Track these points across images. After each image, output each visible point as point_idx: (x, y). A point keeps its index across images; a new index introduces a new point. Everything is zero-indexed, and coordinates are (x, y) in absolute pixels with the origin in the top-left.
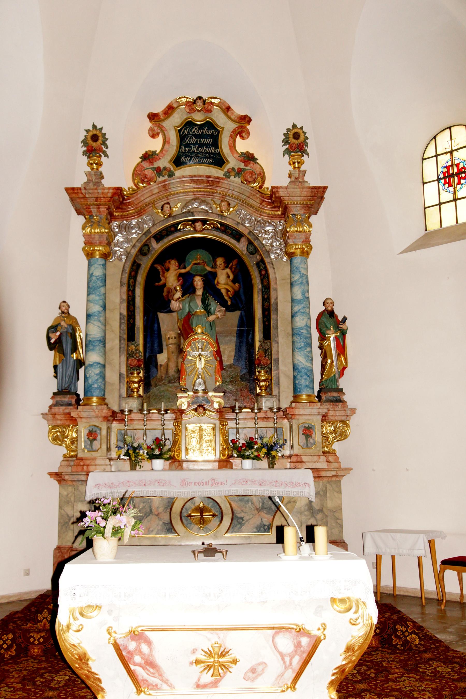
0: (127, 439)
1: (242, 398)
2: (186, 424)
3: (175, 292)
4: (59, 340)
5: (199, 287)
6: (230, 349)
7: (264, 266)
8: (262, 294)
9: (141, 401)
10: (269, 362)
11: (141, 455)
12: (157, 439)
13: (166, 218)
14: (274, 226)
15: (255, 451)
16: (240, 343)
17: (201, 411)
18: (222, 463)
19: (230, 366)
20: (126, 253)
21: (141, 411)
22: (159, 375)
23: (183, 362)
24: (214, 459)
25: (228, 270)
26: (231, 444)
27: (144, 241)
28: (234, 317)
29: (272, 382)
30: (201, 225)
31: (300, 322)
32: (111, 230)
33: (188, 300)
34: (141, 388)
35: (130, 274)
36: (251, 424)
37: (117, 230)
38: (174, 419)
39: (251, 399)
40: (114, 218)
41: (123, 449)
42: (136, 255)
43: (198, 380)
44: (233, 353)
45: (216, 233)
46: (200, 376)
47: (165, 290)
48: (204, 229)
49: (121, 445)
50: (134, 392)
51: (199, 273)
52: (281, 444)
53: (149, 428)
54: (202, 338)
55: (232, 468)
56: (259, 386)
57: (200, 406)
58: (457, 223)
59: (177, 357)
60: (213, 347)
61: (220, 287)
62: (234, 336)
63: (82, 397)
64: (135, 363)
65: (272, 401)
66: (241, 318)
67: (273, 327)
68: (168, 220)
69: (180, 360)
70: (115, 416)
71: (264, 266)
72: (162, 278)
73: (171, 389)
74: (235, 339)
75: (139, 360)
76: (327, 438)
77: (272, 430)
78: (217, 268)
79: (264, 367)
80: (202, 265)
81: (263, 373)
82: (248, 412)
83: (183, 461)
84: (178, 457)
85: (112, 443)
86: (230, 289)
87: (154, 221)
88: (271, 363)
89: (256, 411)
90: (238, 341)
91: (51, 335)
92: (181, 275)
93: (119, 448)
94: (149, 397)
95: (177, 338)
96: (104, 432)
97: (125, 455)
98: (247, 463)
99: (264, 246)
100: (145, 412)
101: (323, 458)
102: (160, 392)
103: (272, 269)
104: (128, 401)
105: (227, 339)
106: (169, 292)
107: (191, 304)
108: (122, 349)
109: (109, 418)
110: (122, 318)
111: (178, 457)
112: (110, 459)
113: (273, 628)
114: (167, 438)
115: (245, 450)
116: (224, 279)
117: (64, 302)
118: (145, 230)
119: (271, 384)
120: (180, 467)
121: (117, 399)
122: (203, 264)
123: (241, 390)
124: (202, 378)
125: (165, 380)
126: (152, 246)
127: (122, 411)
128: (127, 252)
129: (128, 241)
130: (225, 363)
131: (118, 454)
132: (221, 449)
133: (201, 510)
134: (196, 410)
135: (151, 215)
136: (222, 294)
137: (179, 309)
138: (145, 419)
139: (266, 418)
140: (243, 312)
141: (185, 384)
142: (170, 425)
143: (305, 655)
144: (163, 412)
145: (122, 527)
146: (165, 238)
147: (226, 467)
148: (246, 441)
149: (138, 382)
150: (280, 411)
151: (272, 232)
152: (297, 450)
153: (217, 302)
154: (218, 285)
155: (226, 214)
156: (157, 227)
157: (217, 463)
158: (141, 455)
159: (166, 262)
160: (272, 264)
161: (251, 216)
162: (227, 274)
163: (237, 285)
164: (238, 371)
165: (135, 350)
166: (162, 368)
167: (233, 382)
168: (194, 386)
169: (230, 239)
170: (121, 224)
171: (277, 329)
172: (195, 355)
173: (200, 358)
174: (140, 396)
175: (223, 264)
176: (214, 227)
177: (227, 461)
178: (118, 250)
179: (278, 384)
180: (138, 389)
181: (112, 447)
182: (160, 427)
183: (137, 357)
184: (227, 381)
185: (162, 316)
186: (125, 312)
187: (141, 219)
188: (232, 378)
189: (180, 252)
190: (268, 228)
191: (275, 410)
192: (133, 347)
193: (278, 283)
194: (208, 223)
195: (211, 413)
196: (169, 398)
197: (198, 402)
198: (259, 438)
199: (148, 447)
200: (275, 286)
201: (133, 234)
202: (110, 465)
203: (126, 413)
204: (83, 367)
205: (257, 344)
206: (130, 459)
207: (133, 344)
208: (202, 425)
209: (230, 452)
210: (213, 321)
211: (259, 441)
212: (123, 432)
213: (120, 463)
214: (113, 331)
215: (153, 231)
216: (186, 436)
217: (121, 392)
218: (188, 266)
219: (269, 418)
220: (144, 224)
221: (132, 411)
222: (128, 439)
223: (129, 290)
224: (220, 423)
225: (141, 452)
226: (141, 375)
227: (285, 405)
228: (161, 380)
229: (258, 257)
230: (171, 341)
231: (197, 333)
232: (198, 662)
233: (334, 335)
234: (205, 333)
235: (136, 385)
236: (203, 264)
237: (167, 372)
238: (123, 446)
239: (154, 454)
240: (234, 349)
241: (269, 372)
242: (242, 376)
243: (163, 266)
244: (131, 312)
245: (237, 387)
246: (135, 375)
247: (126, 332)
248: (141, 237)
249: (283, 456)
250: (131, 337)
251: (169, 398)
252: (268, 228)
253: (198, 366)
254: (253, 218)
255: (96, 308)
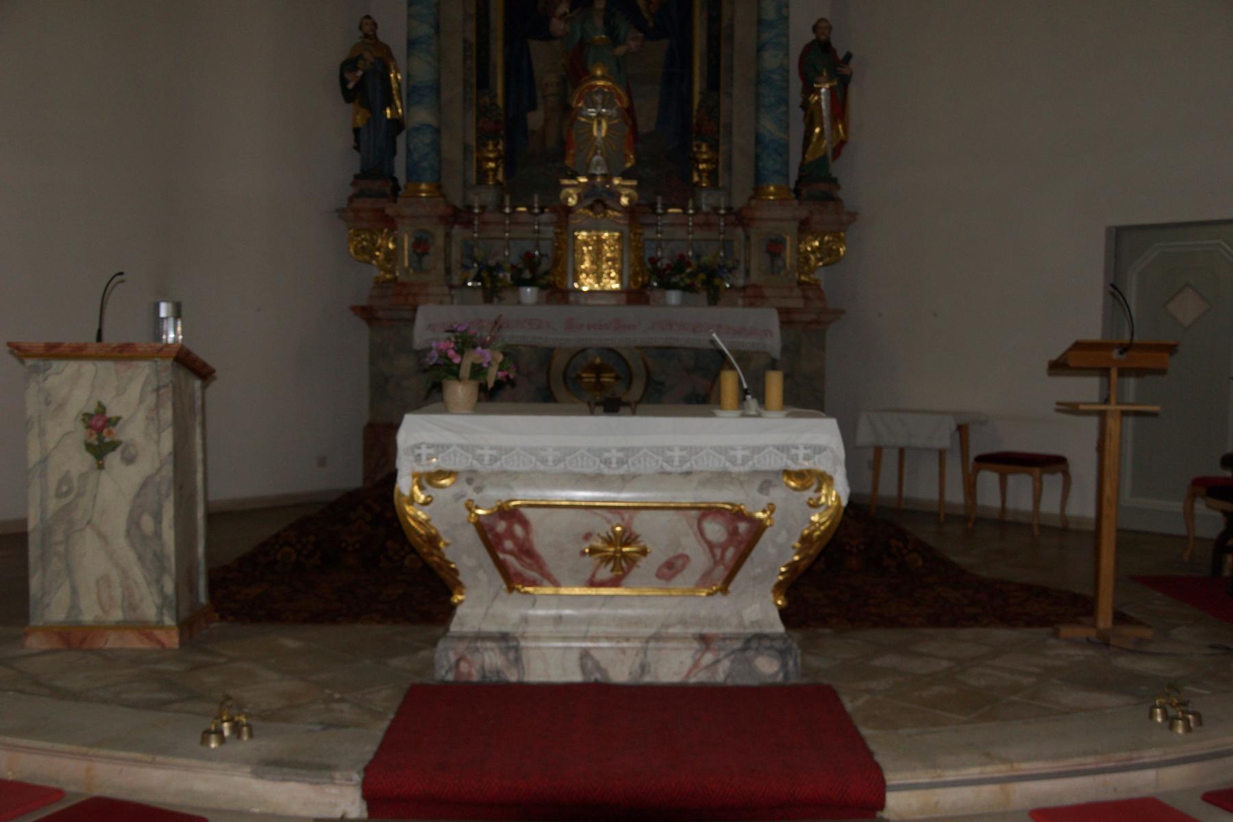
4: (361, 84)
21: (500, 207)
26: (649, 266)
31: (771, 60)
57: (598, 201)
58: (99, 338)
60: (622, 102)
63: (402, 181)
70: (459, 216)
76: (807, 260)
81: (704, 148)
91: (348, 76)
93: (465, 267)
96: (440, 241)
98: (674, 297)
101: (797, 292)
112: (451, 287)
113: (699, 508)
114: (543, 252)
117: (368, 17)
124: (602, 154)
127: (470, 208)
133: (598, 370)
139: (708, 225)
142: (549, 232)
143: (742, 547)
144: (536, 211)
145: (485, 365)
152: (755, 278)
174: (498, 184)
185: (535, 45)
186: (472, 38)
191: (722, 212)
192: (487, 99)
199: (513, 267)
203: (476, 211)
204: (404, 134)
205: (697, 99)
211: (693, 262)
222: (478, 253)
226: (500, 147)
227: (738, 202)
231: (595, 78)
232: (593, 551)
233: (827, 86)
235: (492, 165)
246: (491, 147)
250: (483, 82)
255: (424, 30)
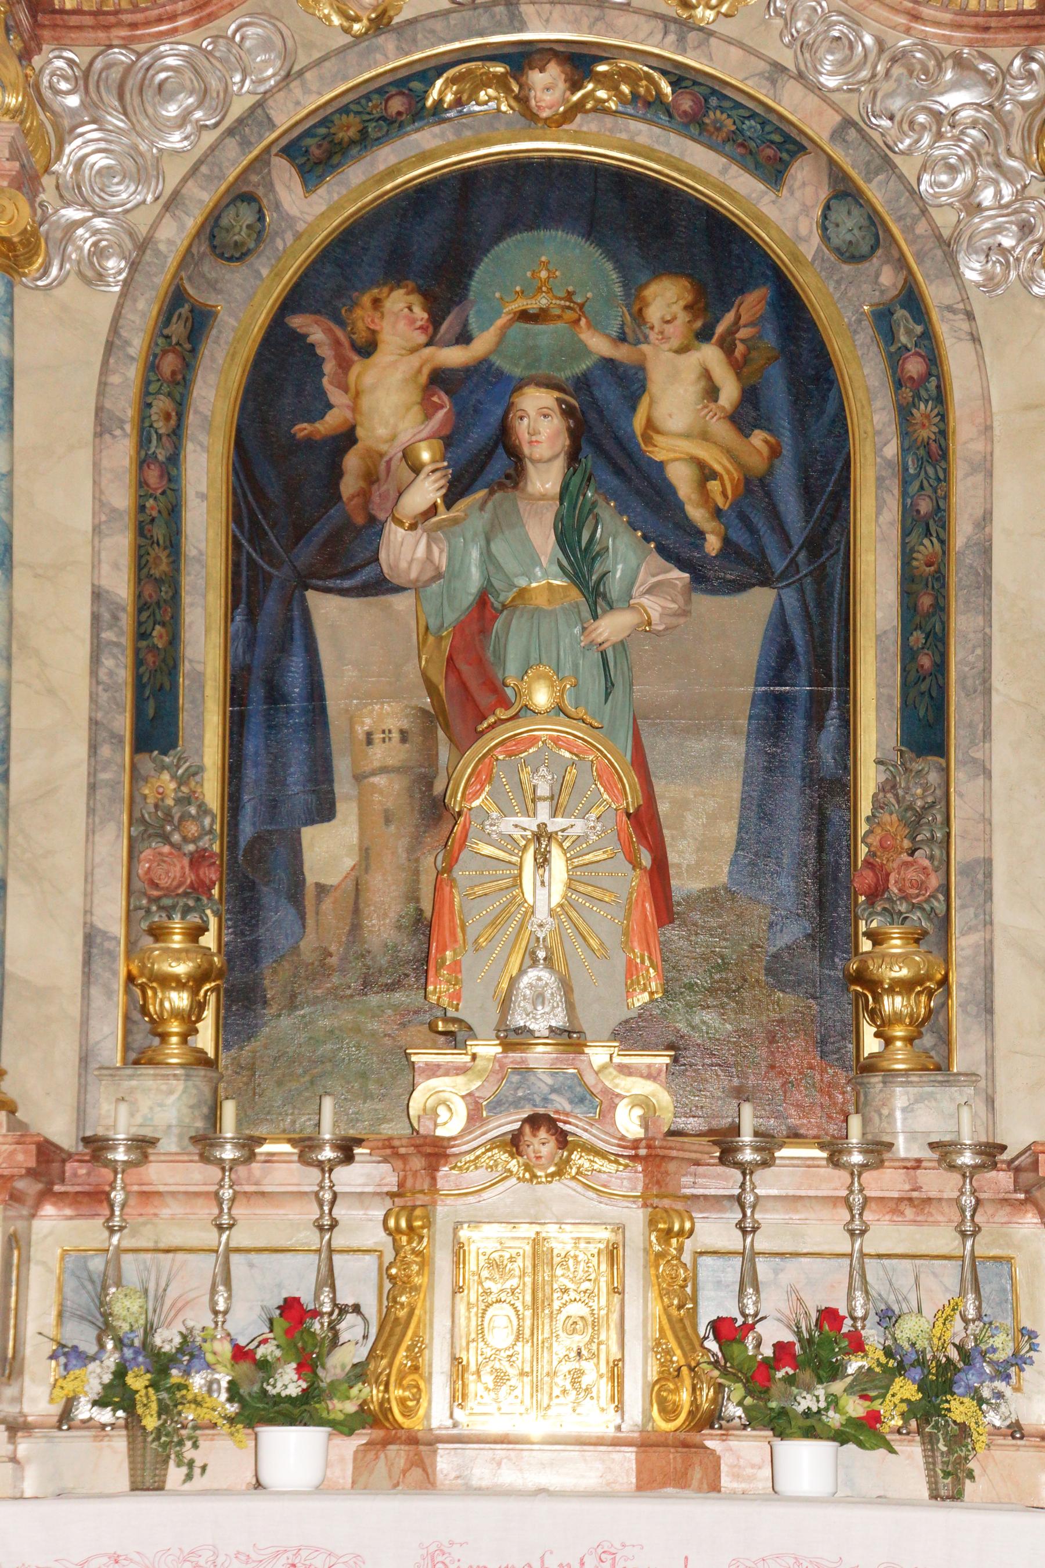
0: (117, 1309)
1: (777, 1084)
2: (457, 1226)
3: (407, 474)
5: (542, 451)
6: (712, 804)
7: (919, 329)
8: (904, 494)
9: (207, 1091)
10: (934, 881)
11: (197, 1402)
12: (291, 1307)
13: (359, 38)
14: (991, 83)
15: (849, 1390)
16: (768, 770)
17: (545, 1151)
18: (656, 1456)
19: (712, 900)
20: (128, 244)
21: (205, 1143)
22: (308, 945)
23: (449, 869)
24: (611, 1432)
25: (710, 354)
26: (712, 1345)
27: (232, 175)
28: (743, 622)
29: (948, 994)
30: (562, 85)
32: (36, 96)
33: (478, 522)
34: (209, 1014)
35: (152, 366)
36: (827, 1231)
37: (73, 101)
38: (392, 1195)
39: (828, 1090)
40: (55, 26)
41: (93, 1366)
42: (188, 258)
43: (532, 975)
44: (729, 830)
45: (644, 132)
46: (541, 954)
47: (352, 461)
48: (578, 108)
49: (84, 1338)
50: (164, 1037)
51: (543, 371)
52: (1001, 1356)
53: (232, 1249)
54: (556, 741)
55: (715, 1487)
56: (874, 1015)
57: (535, 1121)
59: (416, 845)
61: (660, 451)
62: (735, 732)
64: (176, 871)
65: (948, 1106)
66: (780, 623)
67: (962, 679)
68: (370, 51)
69: (430, 862)
71: (919, 329)
72: (335, 396)
73: (374, 1025)
74: (743, 749)
75: (198, 860)
77: (950, 1275)
78: (646, 340)
79: (903, 907)
80: (560, 325)
81: (896, 945)
82: (809, 1163)
83: (433, 1441)
84: (408, 1412)
85: (31, 1328)
86: (717, 461)
87: (287, 55)
88: (946, 889)
89: (857, 1158)
90: (760, 762)
92: (440, 379)
93: (69, 1356)
94: (252, 1068)
95: (417, 739)
97: (100, 1403)
98: (806, 1461)
99: (924, 212)
100: (228, 1153)
102: (314, 1041)
103: (968, 346)
104: (132, 1090)
105: (698, 746)
106: (371, 478)
107: (498, 547)
108: (102, 794)
109: (20, 1185)
110: (106, 616)
111: (408, 1412)
114: (346, 1298)
115: (790, 1380)
116: (686, 404)
118: (237, 109)
119: (944, 1005)
120: (416, 1473)
121: (66, 1072)
122: (570, 315)
123: (772, 1039)
125: (343, 971)
126: (278, 206)
128: (131, 235)
129: (142, 169)
130: (684, 884)
131: (61, 1396)
132: (653, 1375)
134: (514, 1143)
135: (266, 13)
136: (672, 489)
137: (430, 573)
138: (227, 1194)
139: (915, 1204)
140: (791, 598)
141: (457, 996)
142: (364, 1227)
144: (328, 1154)
146: (358, 158)
147: (680, 1480)
148: (798, 1333)
149: (195, 982)
150: (994, 1166)
151: (974, 124)
153: (646, 538)
154: (648, 440)
155: (710, 15)
156: (307, 91)
157: (629, 1455)
158: (197, 1402)
159: (355, 304)
160: (970, 316)
161: (856, 24)
162: (706, 374)
163: (758, 439)
164: (755, 931)
165: (178, 801)
166: (327, 905)
167: (725, 987)
168: (506, 1004)
169: (724, 171)
170: (98, 64)
171: (987, 692)
172: (517, 834)
173: (541, 863)
174: (201, 1061)
175: (683, 317)
176: (635, 95)
177: (685, 1445)
178: (82, 223)
179: (986, 1007)
180: (190, 1020)
181: (29, 1351)
182: (312, 1238)
183: (185, 839)
184: (690, 987)
185: (327, 610)
186: (121, 586)
187: (215, 38)
188: (720, 969)
189: (435, 241)
190: (952, 99)
191: (967, 1159)
192: (167, 782)
193: (997, 431)
194: (602, 68)
195: (599, 1163)
196: (363, 1076)
197: (528, 1099)
198: (873, 1318)
199: (240, 1354)
200: (978, 446)
201: (163, 127)
202: (14, 1459)
203: (120, 1155)
205: (869, 780)
206: (133, 1423)
207: (164, 767)
208: (550, 1230)
209: (707, 1394)
210: (622, 646)
211: (873, 1336)
212: (97, 1264)
213: (74, 1446)
214: (51, 692)
215: (289, 114)
216: (457, 1290)
217: (94, 1037)
218: (483, 329)
219: (929, 1200)
220: (232, 71)
221: (153, 1142)
222: (127, 1309)
223: (143, 462)
224: (652, 1223)
225: (197, 1381)
226: (208, 940)
228: (321, 969)
229: (889, 279)
230: (379, 754)
234: (571, 709)
235: (180, 1000)
236: (570, 315)
237: (356, 928)
238: (92, 1349)
239: (272, 1391)
240: (736, 804)
241: (932, 938)
242: (776, 956)
243: (341, 323)
244: (159, 582)
245: (747, 1021)
246: (177, 941)
247: (127, 696)
248: (213, 148)
249: (1016, 1430)
250: (155, 726)
251: (363, 1076)
252: (952, 99)
253: (530, 901)
254: (868, 40)
